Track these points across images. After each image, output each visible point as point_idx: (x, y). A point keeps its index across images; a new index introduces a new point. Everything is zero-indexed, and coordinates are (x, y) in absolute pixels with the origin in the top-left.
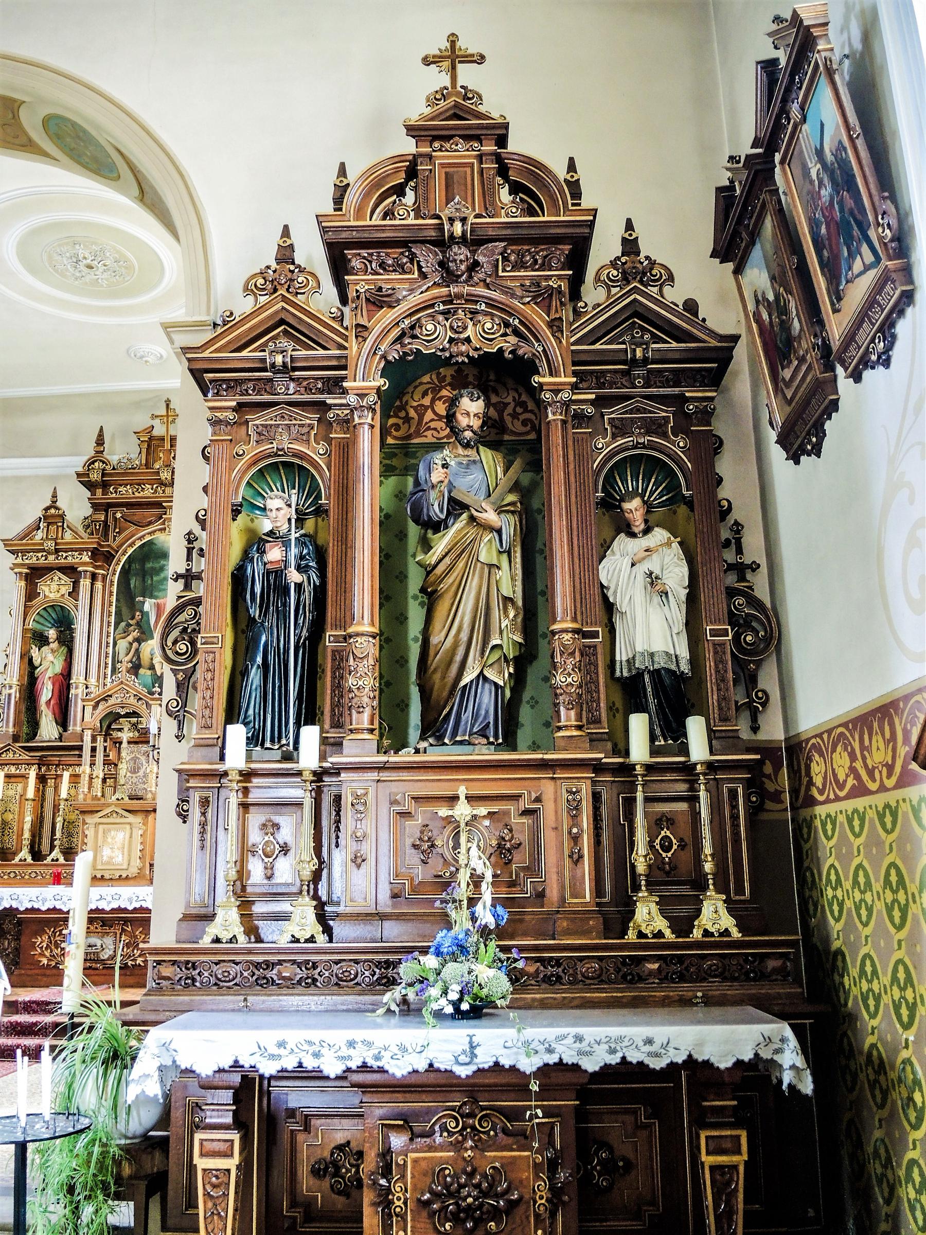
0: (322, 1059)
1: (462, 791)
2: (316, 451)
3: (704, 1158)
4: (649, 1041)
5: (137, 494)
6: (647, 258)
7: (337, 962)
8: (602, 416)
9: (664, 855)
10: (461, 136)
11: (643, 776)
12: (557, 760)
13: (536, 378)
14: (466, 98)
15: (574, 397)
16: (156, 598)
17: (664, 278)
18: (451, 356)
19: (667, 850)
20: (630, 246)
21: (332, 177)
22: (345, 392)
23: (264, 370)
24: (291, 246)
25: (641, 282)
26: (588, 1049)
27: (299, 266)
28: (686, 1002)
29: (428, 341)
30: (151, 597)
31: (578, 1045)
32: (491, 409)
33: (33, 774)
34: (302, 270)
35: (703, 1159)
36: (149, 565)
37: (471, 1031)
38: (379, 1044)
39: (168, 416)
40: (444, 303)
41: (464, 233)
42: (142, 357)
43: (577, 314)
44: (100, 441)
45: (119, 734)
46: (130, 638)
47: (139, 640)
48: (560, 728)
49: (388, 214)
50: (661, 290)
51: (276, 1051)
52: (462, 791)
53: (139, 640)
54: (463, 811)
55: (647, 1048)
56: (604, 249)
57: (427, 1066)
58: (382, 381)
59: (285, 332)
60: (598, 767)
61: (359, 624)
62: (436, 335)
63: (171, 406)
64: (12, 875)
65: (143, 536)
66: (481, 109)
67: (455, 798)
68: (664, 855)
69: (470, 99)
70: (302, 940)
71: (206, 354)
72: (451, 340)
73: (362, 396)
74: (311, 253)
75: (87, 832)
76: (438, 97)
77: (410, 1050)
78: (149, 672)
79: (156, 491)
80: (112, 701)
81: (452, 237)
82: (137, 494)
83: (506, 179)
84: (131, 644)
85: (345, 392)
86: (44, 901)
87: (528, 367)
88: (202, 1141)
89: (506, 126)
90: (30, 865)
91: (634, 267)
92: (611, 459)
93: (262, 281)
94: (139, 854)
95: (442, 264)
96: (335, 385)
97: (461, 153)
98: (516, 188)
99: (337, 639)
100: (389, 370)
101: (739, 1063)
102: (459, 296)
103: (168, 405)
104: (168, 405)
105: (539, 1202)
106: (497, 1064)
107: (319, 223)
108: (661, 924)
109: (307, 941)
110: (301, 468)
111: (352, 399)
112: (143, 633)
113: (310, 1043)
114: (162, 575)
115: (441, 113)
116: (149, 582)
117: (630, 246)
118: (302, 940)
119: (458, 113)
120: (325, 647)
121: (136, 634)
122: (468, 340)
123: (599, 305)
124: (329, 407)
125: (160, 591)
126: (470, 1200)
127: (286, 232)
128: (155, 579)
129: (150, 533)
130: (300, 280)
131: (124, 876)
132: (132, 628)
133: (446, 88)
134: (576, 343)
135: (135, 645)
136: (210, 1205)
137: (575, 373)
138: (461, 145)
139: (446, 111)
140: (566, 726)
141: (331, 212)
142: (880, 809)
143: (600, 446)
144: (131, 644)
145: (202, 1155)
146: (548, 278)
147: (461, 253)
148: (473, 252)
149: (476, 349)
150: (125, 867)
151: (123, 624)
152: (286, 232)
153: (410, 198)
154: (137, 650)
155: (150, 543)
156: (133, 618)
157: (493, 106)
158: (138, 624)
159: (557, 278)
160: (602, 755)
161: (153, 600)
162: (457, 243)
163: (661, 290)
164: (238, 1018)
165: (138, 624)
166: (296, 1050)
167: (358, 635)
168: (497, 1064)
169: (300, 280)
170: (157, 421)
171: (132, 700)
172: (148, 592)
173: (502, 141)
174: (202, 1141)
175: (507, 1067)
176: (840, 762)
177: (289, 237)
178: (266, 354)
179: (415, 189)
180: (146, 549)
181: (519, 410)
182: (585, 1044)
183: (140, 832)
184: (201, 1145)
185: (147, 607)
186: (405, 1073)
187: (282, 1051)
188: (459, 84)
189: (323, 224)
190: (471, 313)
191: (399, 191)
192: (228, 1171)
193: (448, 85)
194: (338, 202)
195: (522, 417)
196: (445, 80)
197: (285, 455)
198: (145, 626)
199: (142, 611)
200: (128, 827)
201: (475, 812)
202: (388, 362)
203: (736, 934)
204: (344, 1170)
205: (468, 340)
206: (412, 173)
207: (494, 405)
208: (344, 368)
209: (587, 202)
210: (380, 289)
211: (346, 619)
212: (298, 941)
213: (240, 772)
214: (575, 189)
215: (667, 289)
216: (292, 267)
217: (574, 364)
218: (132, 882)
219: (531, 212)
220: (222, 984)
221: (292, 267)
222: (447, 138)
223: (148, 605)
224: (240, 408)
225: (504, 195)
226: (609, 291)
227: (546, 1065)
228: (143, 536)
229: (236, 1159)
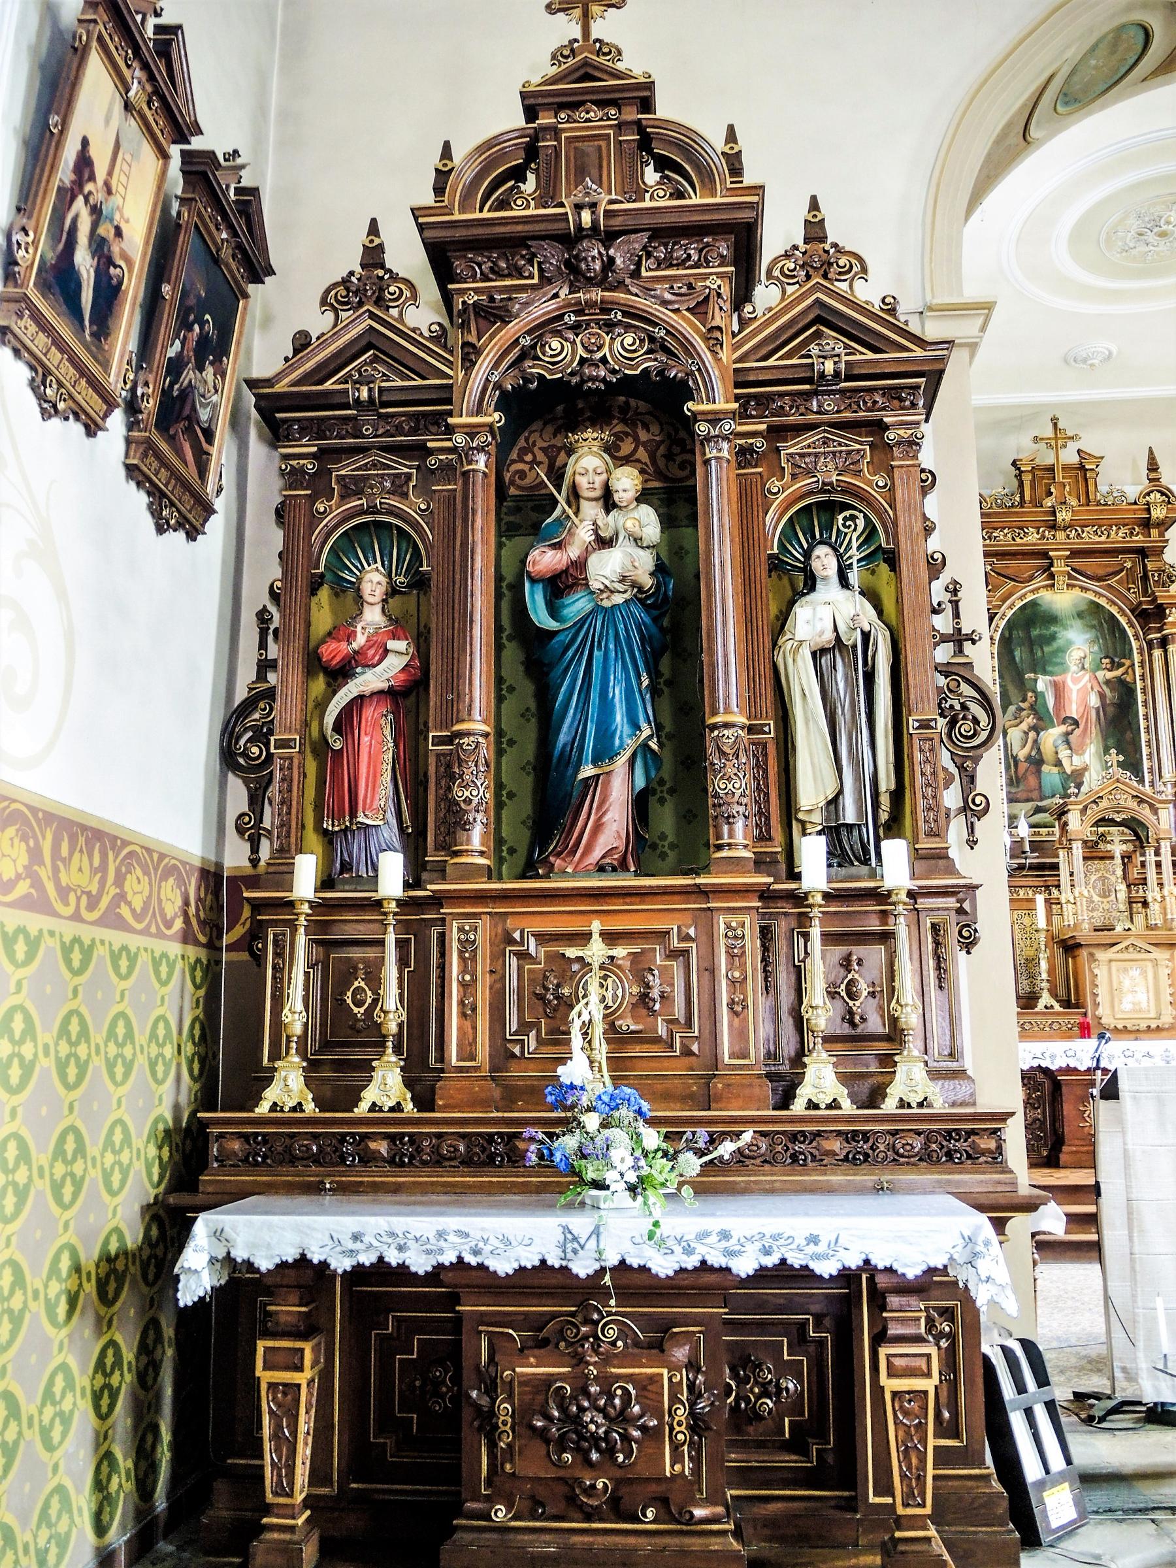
0: (407, 1254)
1: (596, 926)
2: (414, 505)
3: (884, 1380)
4: (814, 1240)
5: (1018, 540)
6: (835, 245)
7: (894, 1133)
8: (778, 451)
9: (356, 1010)
10: (594, 102)
11: (395, 914)
12: (573, 889)
13: (690, 404)
14: (599, 53)
15: (740, 429)
16: (1050, 674)
17: (855, 269)
18: (583, 382)
19: (359, 1004)
20: (815, 231)
21: (434, 159)
22: (450, 430)
23: (346, 406)
24: (381, 247)
25: (825, 276)
26: (738, 1248)
27: (390, 271)
28: (316, 1189)
29: (553, 364)
30: (1045, 673)
31: (724, 1244)
32: (641, 449)
33: (1040, 899)
34: (395, 278)
35: (258, 1374)
36: (1035, 632)
37: (564, 1220)
38: (475, 1234)
39: (1056, 439)
40: (575, 312)
41: (595, 223)
42: (1085, 361)
43: (743, 323)
44: (1153, 467)
45: (1109, 847)
46: (1024, 726)
47: (1036, 729)
48: (719, 848)
49: (503, 204)
50: (851, 286)
51: (350, 1245)
52: (596, 926)
53: (1036, 729)
54: (596, 951)
55: (811, 1249)
56: (779, 234)
57: (861, 1263)
58: (496, 416)
59: (375, 359)
60: (766, 895)
61: (727, 711)
62: (562, 354)
63: (1060, 425)
64: (1055, 1026)
65: (1024, 595)
66: (620, 66)
67: (587, 936)
68: (356, 1010)
69: (605, 54)
70: (823, 1106)
71: (328, 385)
72: (583, 361)
73: (472, 436)
74: (407, 256)
75: (1096, 971)
76: (566, 53)
77: (514, 1243)
78: (1055, 770)
79: (1043, 537)
80: (1104, 804)
81: (579, 227)
82: (1018, 540)
83: (650, 152)
84: (1026, 733)
85: (450, 430)
86: (1053, 1057)
87: (682, 391)
88: (888, 1356)
89: (650, 86)
90: (1058, 1014)
91: (820, 255)
92: (353, 517)
93: (344, 293)
94: (1170, 999)
95: (567, 263)
96: (438, 422)
97: (594, 119)
98: (663, 164)
99: (439, 741)
100: (506, 402)
101: (283, 1265)
102: (591, 304)
103: (1055, 425)
104: (1055, 425)
105: (677, 1429)
106: (623, 1262)
107: (416, 218)
108: (841, 1093)
109: (392, 1109)
110: (378, 525)
111: (459, 439)
112: (1040, 719)
113: (392, 1234)
114: (1055, 645)
115: (570, 74)
116: (1039, 654)
117: (815, 231)
118: (823, 1106)
119: (586, 72)
120: (427, 750)
121: (1031, 720)
122: (604, 360)
123: (770, 309)
124: (431, 452)
125: (1057, 664)
126: (593, 1427)
127: (374, 228)
128: (1046, 649)
129: (1032, 591)
130: (392, 289)
131: (1153, 1026)
132: (1024, 713)
133: (576, 40)
134: (740, 360)
135: (1032, 734)
136: (901, 1434)
137: (737, 398)
138: (595, 113)
139: (577, 70)
140: (729, 845)
141: (431, 203)
142: (157, 955)
143: (775, 490)
144: (1026, 733)
145: (890, 1375)
146: (705, 277)
147: (593, 251)
148: (607, 249)
149: (614, 372)
150: (1153, 1015)
151: (1012, 708)
152: (374, 228)
153: (530, 185)
154: (1035, 741)
155: (1034, 604)
156: (1024, 700)
157: (634, 63)
158: (1032, 708)
159: (717, 279)
160: (771, 880)
161: (1048, 678)
162: (587, 236)
163: (851, 286)
164: (870, 1201)
165: (1032, 708)
166: (376, 1243)
167: (726, 725)
168: (623, 1262)
169: (392, 289)
170: (1042, 445)
171: (1132, 804)
172: (1040, 666)
173: (647, 105)
174: (888, 1356)
175: (635, 1266)
176: (170, 895)
177: (378, 235)
178: (349, 386)
179: (537, 172)
180: (1028, 611)
181: (676, 449)
182: (733, 1241)
183: (1168, 971)
184: (889, 1363)
185: (1040, 686)
186: (919, 1272)
187: (358, 1246)
188: (594, 36)
189: (421, 220)
190: (605, 325)
191: (518, 174)
192: (299, 1386)
193: (579, 36)
194: (439, 190)
195: (679, 459)
196: (576, 32)
197: (379, 513)
198: (1041, 711)
199: (1034, 691)
200: (1149, 964)
201: (611, 953)
202: (504, 393)
203: (310, 1108)
204: (756, 1390)
205: (604, 360)
206: (532, 152)
207: (644, 444)
208: (449, 401)
209: (748, 179)
210: (492, 299)
211: (453, 711)
212: (909, 1106)
213: (397, 901)
214: (735, 164)
215: (859, 284)
216: (381, 273)
217: (737, 385)
218: (1164, 1034)
219: (680, 195)
220: (748, 1162)
221: (381, 273)
222: (574, 106)
223: (1042, 683)
224: (322, 455)
225: (651, 176)
226: (784, 291)
227: (762, 1268)
228: (1024, 595)
229: (935, 1379)
